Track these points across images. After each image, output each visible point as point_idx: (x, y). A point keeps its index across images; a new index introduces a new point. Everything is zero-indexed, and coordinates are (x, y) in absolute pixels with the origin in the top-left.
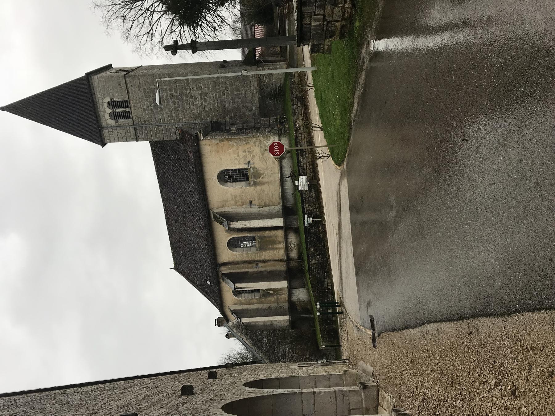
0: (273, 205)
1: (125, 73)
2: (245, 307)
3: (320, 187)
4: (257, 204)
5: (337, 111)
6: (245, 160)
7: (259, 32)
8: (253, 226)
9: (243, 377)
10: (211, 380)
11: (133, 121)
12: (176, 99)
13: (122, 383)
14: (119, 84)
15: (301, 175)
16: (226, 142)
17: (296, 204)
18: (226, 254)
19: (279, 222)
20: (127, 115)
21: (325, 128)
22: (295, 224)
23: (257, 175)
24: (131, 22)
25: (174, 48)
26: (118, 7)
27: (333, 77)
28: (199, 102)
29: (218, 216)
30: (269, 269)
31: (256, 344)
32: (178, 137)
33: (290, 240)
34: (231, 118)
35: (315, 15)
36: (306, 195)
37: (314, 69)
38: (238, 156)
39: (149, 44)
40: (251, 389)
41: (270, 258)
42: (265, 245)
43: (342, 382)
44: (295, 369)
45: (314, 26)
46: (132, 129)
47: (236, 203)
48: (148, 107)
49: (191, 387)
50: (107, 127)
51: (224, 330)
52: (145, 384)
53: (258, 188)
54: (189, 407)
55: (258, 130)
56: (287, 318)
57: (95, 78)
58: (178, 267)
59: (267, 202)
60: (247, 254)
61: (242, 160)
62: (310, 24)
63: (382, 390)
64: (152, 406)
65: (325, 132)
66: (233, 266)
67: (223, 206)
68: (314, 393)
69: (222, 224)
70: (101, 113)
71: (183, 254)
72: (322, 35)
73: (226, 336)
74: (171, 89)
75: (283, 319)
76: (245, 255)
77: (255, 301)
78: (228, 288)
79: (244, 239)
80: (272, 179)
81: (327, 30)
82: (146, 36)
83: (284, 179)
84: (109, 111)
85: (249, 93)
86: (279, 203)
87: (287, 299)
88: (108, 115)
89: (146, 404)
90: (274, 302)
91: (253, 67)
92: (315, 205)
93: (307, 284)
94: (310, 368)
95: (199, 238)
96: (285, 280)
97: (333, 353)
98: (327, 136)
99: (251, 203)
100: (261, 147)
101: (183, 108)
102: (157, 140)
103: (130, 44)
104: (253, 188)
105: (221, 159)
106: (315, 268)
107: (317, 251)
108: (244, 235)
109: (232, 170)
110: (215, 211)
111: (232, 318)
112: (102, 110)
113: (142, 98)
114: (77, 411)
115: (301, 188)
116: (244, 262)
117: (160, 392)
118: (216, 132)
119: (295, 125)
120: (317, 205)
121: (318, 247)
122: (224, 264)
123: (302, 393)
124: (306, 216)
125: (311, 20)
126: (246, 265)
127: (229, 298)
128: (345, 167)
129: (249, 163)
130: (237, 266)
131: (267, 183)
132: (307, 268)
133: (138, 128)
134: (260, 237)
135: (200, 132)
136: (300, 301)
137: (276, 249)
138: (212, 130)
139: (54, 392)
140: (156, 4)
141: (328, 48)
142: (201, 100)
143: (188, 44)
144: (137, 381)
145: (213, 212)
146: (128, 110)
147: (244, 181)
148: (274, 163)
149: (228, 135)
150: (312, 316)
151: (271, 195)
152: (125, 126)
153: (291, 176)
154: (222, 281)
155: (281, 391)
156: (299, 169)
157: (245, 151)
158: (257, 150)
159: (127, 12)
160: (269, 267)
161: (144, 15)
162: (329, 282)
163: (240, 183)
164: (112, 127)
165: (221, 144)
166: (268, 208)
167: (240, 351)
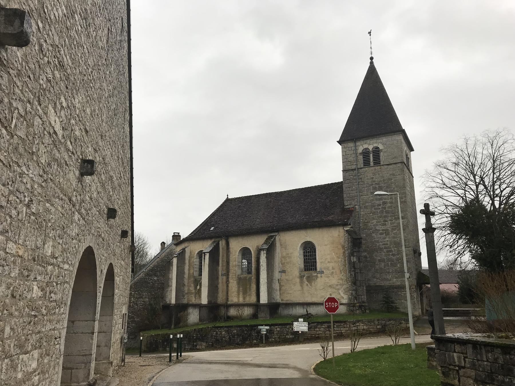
1: (406, 163)
2: (187, 262)
3: (296, 344)
5: (369, 371)
6: (325, 268)
7: (451, 288)
8: (261, 273)
9: (120, 262)
10: (120, 232)
11: (361, 168)
12: (382, 207)
13: (129, 156)
14: (395, 157)
15: (309, 324)
16: (342, 251)
17: (281, 317)
18: (236, 245)
19: (264, 299)
20: (367, 163)
21: (354, 355)
22: (261, 315)
23: (310, 279)
24: (454, 170)
25: (427, 212)
26: (467, 159)
27: (403, 369)
28: (380, 228)
29: (272, 240)
30: (220, 286)
31: (152, 270)
32: (347, 207)
33: (246, 308)
34: (365, 257)
35: (465, 358)
36: (288, 329)
37: (413, 347)
38: (329, 262)
39: (434, 185)
40: (105, 271)
41: (230, 288)
42: (243, 284)
43: (102, 359)
44: (121, 311)
45: (453, 355)
46: (354, 167)
47: (283, 257)
48: (374, 182)
49: (114, 217)
50: (356, 146)
51: (169, 240)
52: (124, 175)
53: (298, 280)
54: (95, 216)
55: (354, 283)
56: (173, 301)
57: (401, 137)
58: (228, 201)
59: (283, 288)
60: (236, 266)
62: (455, 352)
64: (101, 184)
65: (349, 355)
66: (225, 252)
67: (281, 245)
68: (93, 333)
69: (264, 243)
70: (368, 141)
71: (239, 206)
72: (445, 364)
73: (163, 243)
74: (391, 203)
75: (172, 298)
76: (234, 263)
77: (192, 271)
78: (206, 246)
79: (249, 263)
81: (450, 370)
82: (441, 182)
83: (305, 307)
84: (371, 148)
85: (389, 277)
86: (282, 300)
87: (191, 303)
88: (367, 147)
89: (103, 179)
90: (189, 290)
91: (415, 282)
92: (279, 338)
94: (120, 326)
95: (253, 222)
96: (208, 301)
97: (132, 347)
98: (346, 357)
99: (283, 272)
100: (337, 285)
101: (374, 213)
102: (344, 188)
103: (433, 168)
104: (298, 274)
105: (326, 245)
106: (217, 334)
107: (233, 337)
108: (253, 263)
109: (315, 255)
110: (277, 237)
111: (179, 249)
112: (372, 142)
113: (383, 177)
114: (107, 123)
115: (295, 324)
116: (228, 263)
117: (114, 189)
118: (351, 242)
119: (358, 321)
121: (237, 338)
122: (228, 244)
123: (94, 321)
124: (268, 328)
125: (458, 352)
126: (225, 264)
127: (197, 247)
128: (312, 376)
129: (322, 272)
130: (225, 255)
131: (303, 289)
132: (218, 325)
133: (355, 172)
134: (250, 278)
135: (351, 227)
136: (187, 315)
137: (239, 294)
138: (354, 239)
139: (128, 102)
140: (472, 193)
141: (433, 366)
142: (382, 230)
143: (431, 224)
144: (128, 168)
145: (276, 236)
146: (372, 164)
147: (305, 266)
149: (349, 253)
150: (173, 327)
151: (291, 292)
152: (357, 161)
153: (308, 314)
154: (213, 240)
155: (99, 300)
156: (315, 322)
157: (333, 269)
158: (334, 281)
159: (463, 166)
160: (221, 286)
161: (461, 182)
162: (203, 347)
163: (303, 262)
164: (356, 150)
165: (340, 247)
166: (278, 288)
167: (149, 253)
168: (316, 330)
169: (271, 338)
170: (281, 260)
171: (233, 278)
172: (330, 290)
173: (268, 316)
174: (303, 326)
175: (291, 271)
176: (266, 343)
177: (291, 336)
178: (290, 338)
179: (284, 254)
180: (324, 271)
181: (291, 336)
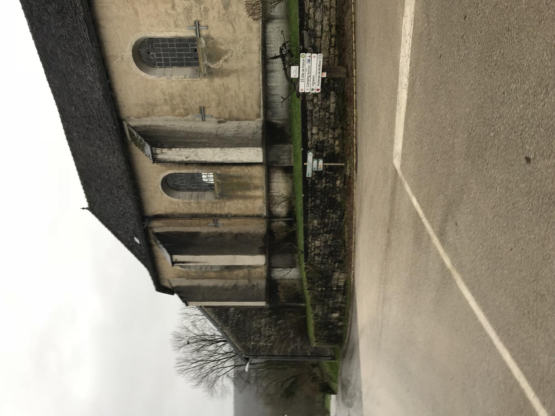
0: (246, 120)
2: (196, 283)
4: (216, 115)
6: (188, 18)
15: (305, 51)
17: (289, 120)
22: (285, 160)
23: (215, 54)
29: (135, 133)
36: (314, 105)
38: (173, 7)
47: (173, 110)
53: (217, 81)
59: (235, 113)
60: (198, 203)
61: (182, 17)
63: (313, 125)
66: (174, 221)
67: (148, 115)
71: (96, 190)
76: (194, 205)
78: (163, 255)
80: (244, 63)
86: (258, 116)
87: (265, 274)
92: (334, 129)
93: (299, 262)
96: (260, 253)
99: (202, 111)
104: (206, 80)
105: (136, 13)
106: (318, 255)
107: (326, 225)
109: (163, 40)
110: (132, 124)
115: (303, 87)
116: (194, 216)
120: (338, 131)
121: (329, 218)
122: (158, 217)
124: (310, 156)
129: (197, 24)
130: (180, 221)
131: (235, 71)
137: (250, 197)
145: (128, 125)
148: (250, 29)
150: (303, 305)
156: (301, 35)
160: (237, 227)
166: (235, 123)
168: (319, 34)
169: (332, 147)
170: (180, 115)
171: (220, 207)
172: (233, 8)
173: (287, 147)
174: (310, 67)
175: (199, 95)
176: (344, 160)
177: (333, 100)
178: (337, 103)
179: (167, 108)
180: (194, 19)
181: (333, 100)
